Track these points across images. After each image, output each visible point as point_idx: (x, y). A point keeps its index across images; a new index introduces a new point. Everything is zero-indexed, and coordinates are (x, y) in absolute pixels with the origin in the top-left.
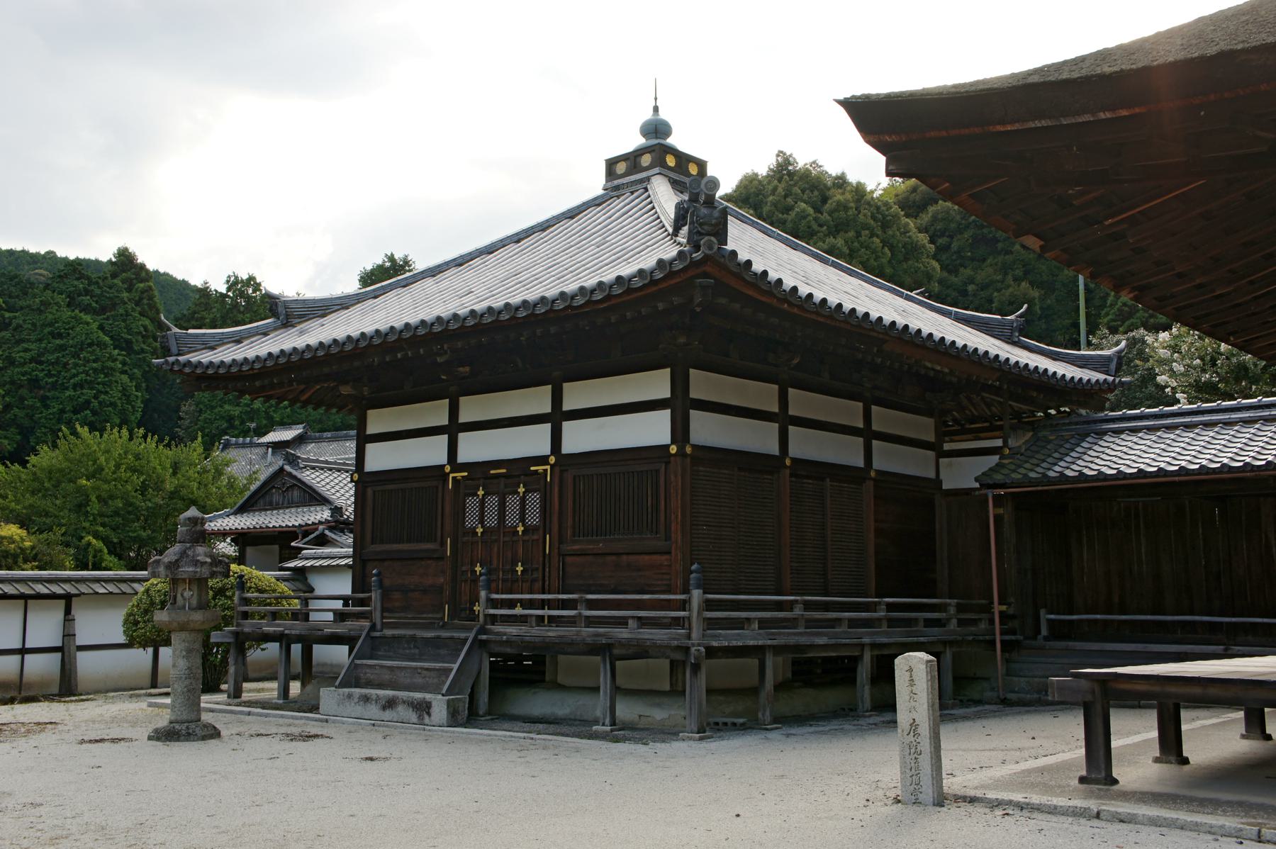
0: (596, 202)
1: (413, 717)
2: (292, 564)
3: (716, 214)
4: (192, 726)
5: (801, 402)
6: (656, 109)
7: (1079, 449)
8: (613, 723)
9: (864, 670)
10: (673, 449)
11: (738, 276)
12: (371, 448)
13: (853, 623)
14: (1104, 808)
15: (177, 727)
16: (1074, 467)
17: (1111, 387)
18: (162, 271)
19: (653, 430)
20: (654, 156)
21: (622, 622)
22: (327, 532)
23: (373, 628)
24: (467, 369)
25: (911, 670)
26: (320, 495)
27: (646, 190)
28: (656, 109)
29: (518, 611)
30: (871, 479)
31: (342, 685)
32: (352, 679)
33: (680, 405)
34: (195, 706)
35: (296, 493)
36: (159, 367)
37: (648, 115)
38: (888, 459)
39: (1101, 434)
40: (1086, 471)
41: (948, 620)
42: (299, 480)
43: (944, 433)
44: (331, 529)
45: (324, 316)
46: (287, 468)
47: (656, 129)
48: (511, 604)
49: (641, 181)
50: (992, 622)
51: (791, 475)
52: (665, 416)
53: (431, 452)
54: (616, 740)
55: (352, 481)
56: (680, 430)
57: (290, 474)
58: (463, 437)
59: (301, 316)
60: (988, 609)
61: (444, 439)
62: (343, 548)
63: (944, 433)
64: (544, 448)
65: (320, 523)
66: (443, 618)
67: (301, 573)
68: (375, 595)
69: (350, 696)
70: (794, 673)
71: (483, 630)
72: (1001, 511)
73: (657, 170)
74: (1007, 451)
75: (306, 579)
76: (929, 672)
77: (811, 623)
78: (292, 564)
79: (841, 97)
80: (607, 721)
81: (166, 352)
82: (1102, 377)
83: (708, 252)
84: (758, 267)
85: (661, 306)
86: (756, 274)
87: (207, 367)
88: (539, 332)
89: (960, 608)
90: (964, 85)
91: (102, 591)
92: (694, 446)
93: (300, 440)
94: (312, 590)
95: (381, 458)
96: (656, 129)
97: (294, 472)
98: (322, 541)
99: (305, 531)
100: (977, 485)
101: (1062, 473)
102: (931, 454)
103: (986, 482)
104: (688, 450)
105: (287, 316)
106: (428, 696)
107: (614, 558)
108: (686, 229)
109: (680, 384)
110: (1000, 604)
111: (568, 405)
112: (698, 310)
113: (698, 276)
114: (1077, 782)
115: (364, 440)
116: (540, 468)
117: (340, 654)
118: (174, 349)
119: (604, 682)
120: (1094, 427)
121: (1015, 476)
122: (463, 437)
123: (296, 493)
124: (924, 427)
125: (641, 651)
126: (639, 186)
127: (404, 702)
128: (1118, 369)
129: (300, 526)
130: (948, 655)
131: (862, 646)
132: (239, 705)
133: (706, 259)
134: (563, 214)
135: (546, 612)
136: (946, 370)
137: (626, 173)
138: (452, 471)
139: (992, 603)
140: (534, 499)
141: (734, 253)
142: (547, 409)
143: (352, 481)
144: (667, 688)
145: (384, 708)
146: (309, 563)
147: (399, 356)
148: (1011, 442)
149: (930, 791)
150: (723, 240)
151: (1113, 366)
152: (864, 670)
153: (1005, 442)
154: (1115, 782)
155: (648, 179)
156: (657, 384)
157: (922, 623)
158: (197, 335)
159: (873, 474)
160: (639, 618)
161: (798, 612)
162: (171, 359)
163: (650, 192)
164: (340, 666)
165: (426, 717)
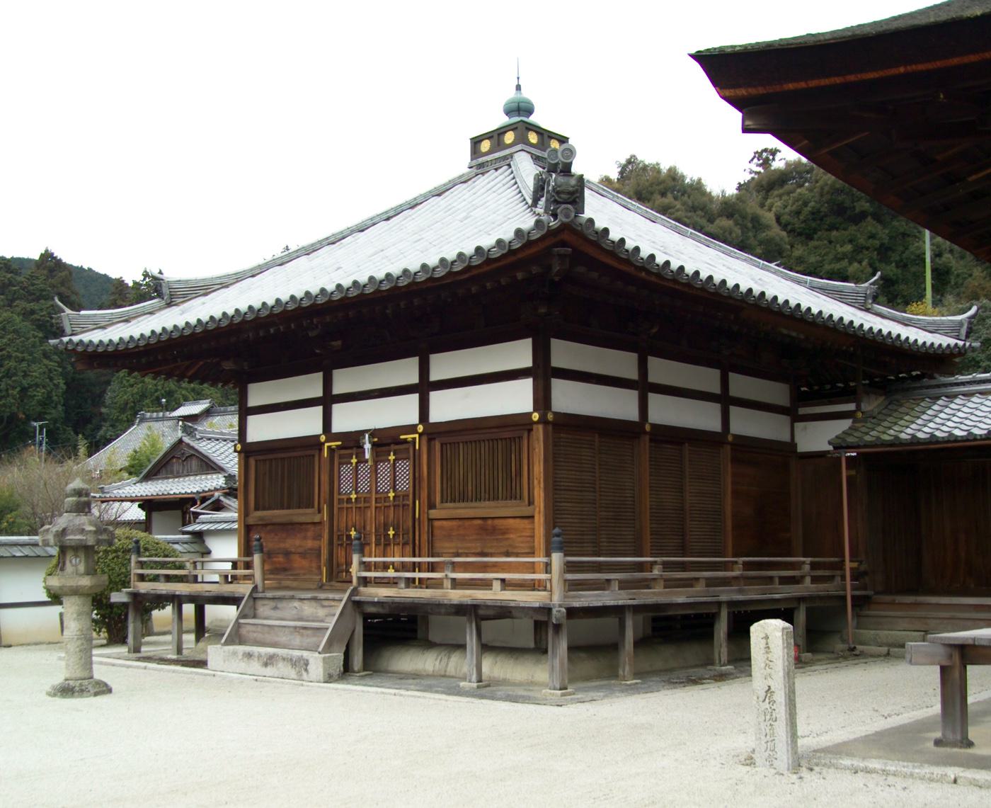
0: (464, 180)
1: (292, 673)
2: (190, 528)
3: (573, 182)
4: (86, 682)
5: (661, 371)
6: (518, 88)
7: (930, 412)
8: (480, 681)
9: (722, 628)
10: (536, 417)
11: (596, 245)
12: (252, 420)
13: (711, 583)
14: (961, 774)
15: (71, 683)
16: (926, 429)
17: (961, 352)
18: (86, 267)
19: (515, 399)
20: (518, 132)
21: (487, 585)
22: (222, 498)
23: (255, 589)
24: (339, 343)
25: (767, 637)
26: (215, 463)
27: (509, 166)
28: (518, 88)
29: (391, 573)
30: (728, 443)
31: (226, 643)
32: (237, 637)
33: (543, 374)
34: (88, 664)
35: (194, 463)
36: (56, 347)
37: (511, 94)
38: (746, 424)
39: (952, 397)
40: (938, 434)
41: (803, 577)
42: (197, 451)
43: (800, 398)
44: (226, 495)
45: (205, 295)
46: (186, 440)
47: (520, 109)
48: (385, 567)
49: (505, 158)
50: (843, 578)
51: (651, 440)
52: (527, 385)
53: (306, 424)
54: (482, 697)
55: (235, 451)
56: (542, 398)
57: (188, 445)
58: (337, 409)
59: (184, 296)
60: (840, 566)
61: (319, 410)
62: (232, 514)
63: (800, 398)
64: (412, 417)
65: (216, 490)
66: (321, 579)
67: (199, 536)
68: (257, 559)
69: (235, 653)
70: (654, 629)
71: (355, 592)
72: (853, 473)
73: (519, 147)
74: (859, 415)
75: (204, 542)
76: (786, 641)
77: (669, 583)
78: (190, 528)
79: (693, 52)
80: (474, 677)
81: (60, 332)
82: (952, 342)
83: (565, 220)
84: (614, 236)
85: (520, 276)
86: (613, 242)
87: (77, 344)
88: (402, 304)
89: (814, 566)
90: (823, 34)
91: (18, 554)
92: (556, 414)
93: (207, 413)
94: (209, 552)
95: (263, 429)
96: (520, 109)
97: (192, 444)
98: (218, 506)
99: (203, 498)
100: (831, 448)
101: (878, 438)
102: (785, 419)
103: (840, 445)
104: (550, 417)
105: (172, 296)
106: (305, 654)
107: (479, 522)
108: (543, 199)
109: (541, 353)
110: (851, 561)
111: (434, 377)
112: (557, 279)
113: (556, 245)
114: (932, 743)
115: (245, 413)
116: (409, 437)
117: (229, 612)
118: (68, 330)
119: (471, 641)
120: (944, 390)
121: (868, 438)
122: (337, 409)
123: (194, 463)
124: (776, 392)
125: (503, 612)
126: (502, 163)
127: (284, 659)
128: (967, 336)
129: (198, 492)
130: (801, 616)
131: (719, 604)
132: (139, 659)
133: (564, 227)
134: (430, 192)
135: (417, 575)
136: (802, 336)
137: (488, 151)
138: (327, 441)
139: (844, 561)
140: (404, 468)
141: (591, 221)
142: (415, 379)
143: (235, 451)
144: (532, 645)
145: (266, 665)
146: (205, 527)
147: (272, 331)
148: (865, 407)
149: (785, 757)
150: (581, 210)
151: (964, 331)
152: (722, 628)
153: (858, 407)
154: (970, 744)
155: (511, 156)
156: (519, 354)
157: (777, 580)
158: (89, 316)
159: (648, 428)
160: (503, 580)
161: (656, 572)
162: (65, 339)
163: (513, 168)
164: (229, 621)
165: (304, 674)
